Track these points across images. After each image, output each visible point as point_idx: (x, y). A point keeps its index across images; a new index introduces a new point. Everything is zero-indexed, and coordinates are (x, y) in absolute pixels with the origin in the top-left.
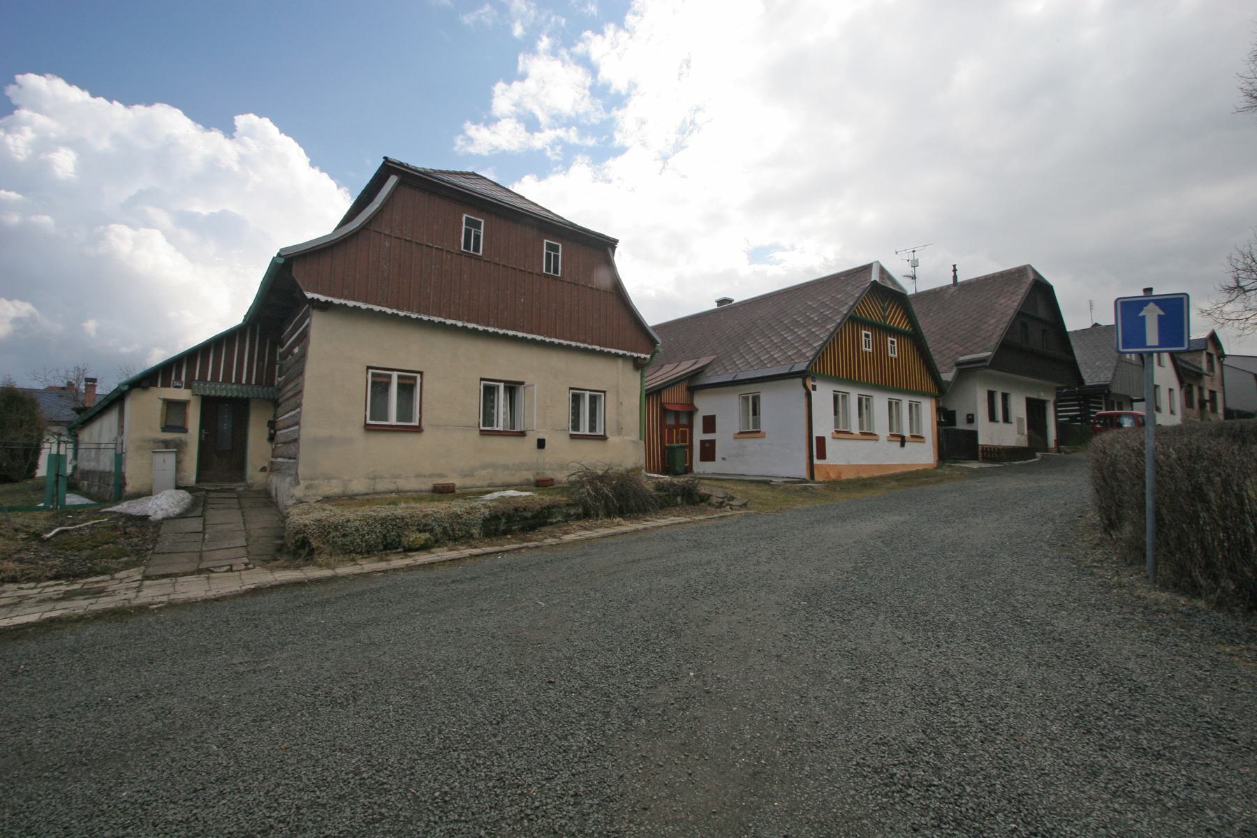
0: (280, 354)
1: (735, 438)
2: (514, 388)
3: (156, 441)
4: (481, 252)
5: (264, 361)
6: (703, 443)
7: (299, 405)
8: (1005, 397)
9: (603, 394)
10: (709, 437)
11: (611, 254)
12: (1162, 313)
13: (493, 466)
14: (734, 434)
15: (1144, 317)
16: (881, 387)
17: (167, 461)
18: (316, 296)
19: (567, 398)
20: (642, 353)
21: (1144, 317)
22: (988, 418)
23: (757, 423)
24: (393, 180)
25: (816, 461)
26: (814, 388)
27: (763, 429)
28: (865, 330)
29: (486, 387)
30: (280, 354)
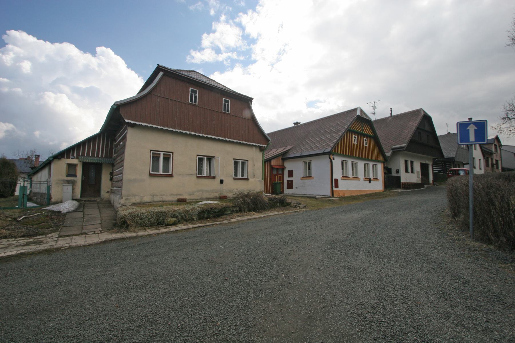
0: (115, 145)
1: (301, 179)
2: (210, 159)
3: (64, 181)
4: (197, 103)
5: (108, 148)
6: (288, 181)
7: (123, 166)
8: (412, 163)
9: (247, 161)
10: (290, 179)
11: (250, 104)
12: (476, 128)
13: (202, 191)
14: (301, 178)
15: (469, 130)
16: (361, 158)
17: (69, 189)
18: (129, 121)
19: (232, 163)
20: (263, 144)
21: (469, 130)
22: (405, 171)
23: (310, 173)
24: (161, 74)
25: (334, 189)
26: (334, 159)
27: (312, 175)
28: (354, 135)
29: (199, 159)
30: (115, 145)
